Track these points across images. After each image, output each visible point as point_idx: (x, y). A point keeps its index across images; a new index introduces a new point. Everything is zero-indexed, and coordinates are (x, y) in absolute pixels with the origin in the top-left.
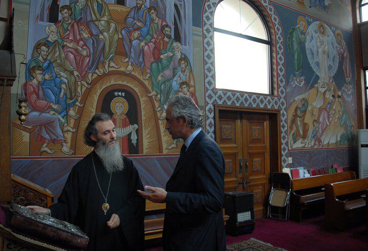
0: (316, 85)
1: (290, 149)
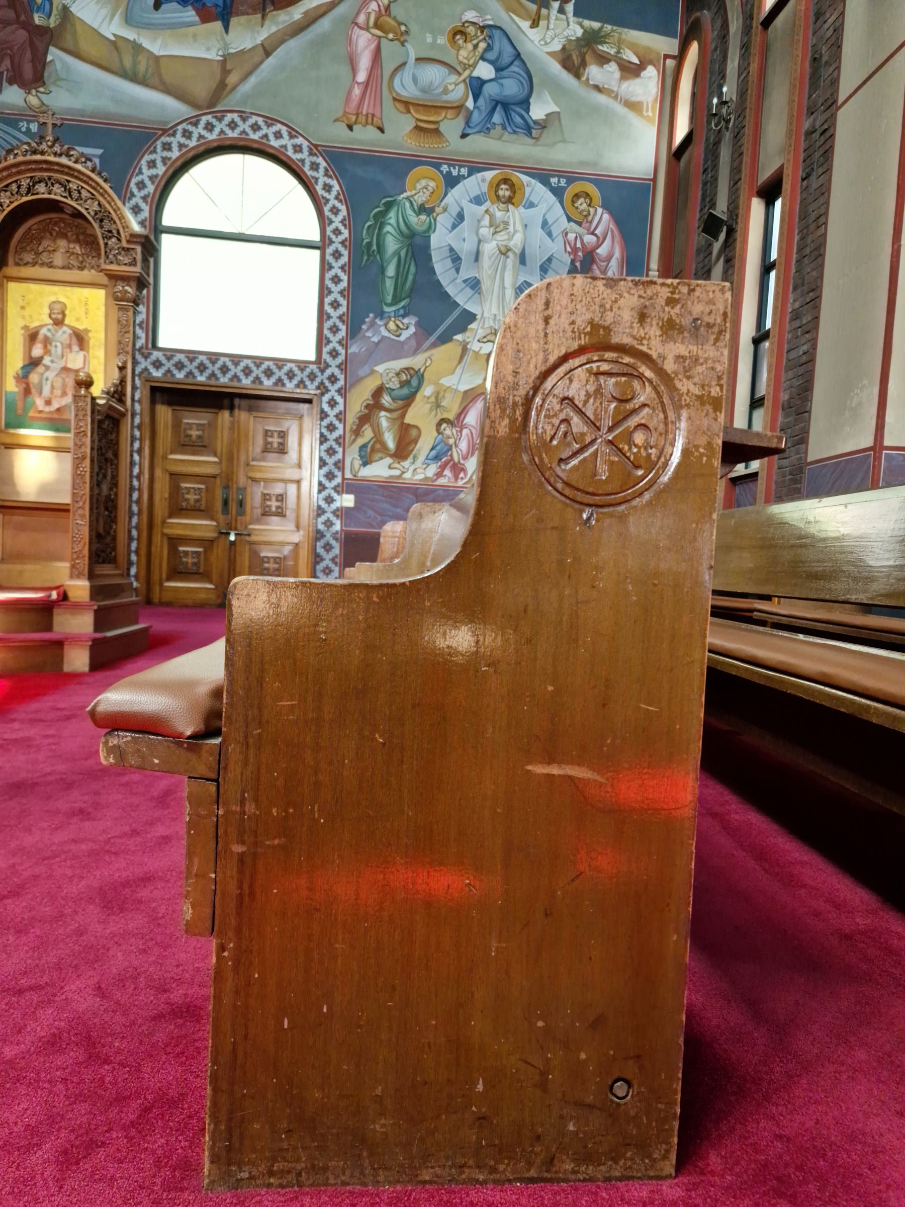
0: (459, 337)
1: (348, 475)
